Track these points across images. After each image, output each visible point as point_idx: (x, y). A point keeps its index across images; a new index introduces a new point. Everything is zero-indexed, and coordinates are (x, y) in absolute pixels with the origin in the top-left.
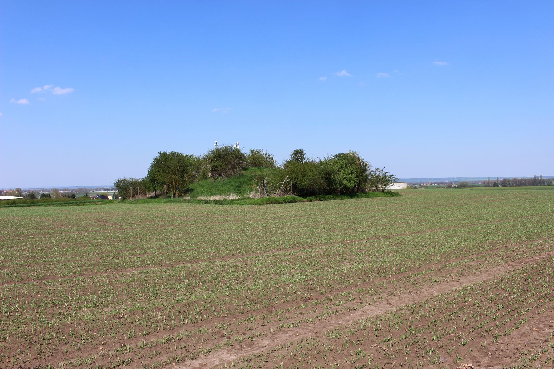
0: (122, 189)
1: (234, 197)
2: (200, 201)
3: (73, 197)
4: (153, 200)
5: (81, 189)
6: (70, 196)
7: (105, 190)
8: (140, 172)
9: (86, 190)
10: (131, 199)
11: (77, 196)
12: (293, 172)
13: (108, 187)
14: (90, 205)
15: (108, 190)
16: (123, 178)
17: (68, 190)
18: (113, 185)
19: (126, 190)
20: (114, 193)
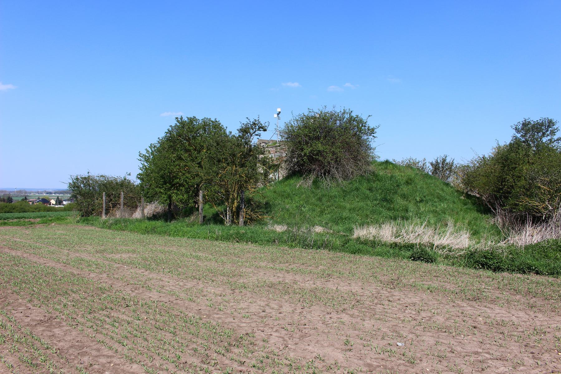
0: (83, 195)
1: (459, 240)
2: (371, 247)
3: (10, 200)
4: (159, 223)
5: (20, 192)
6: (6, 198)
7: (47, 193)
8: (125, 164)
9: (26, 192)
10: (104, 217)
11: (14, 198)
12: (411, 180)
13: (51, 191)
14: (18, 224)
15: (51, 193)
16: (86, 175)
17: (5, 191)
18: (65, 187)
19: (92, 199)
20: (58, 197)
